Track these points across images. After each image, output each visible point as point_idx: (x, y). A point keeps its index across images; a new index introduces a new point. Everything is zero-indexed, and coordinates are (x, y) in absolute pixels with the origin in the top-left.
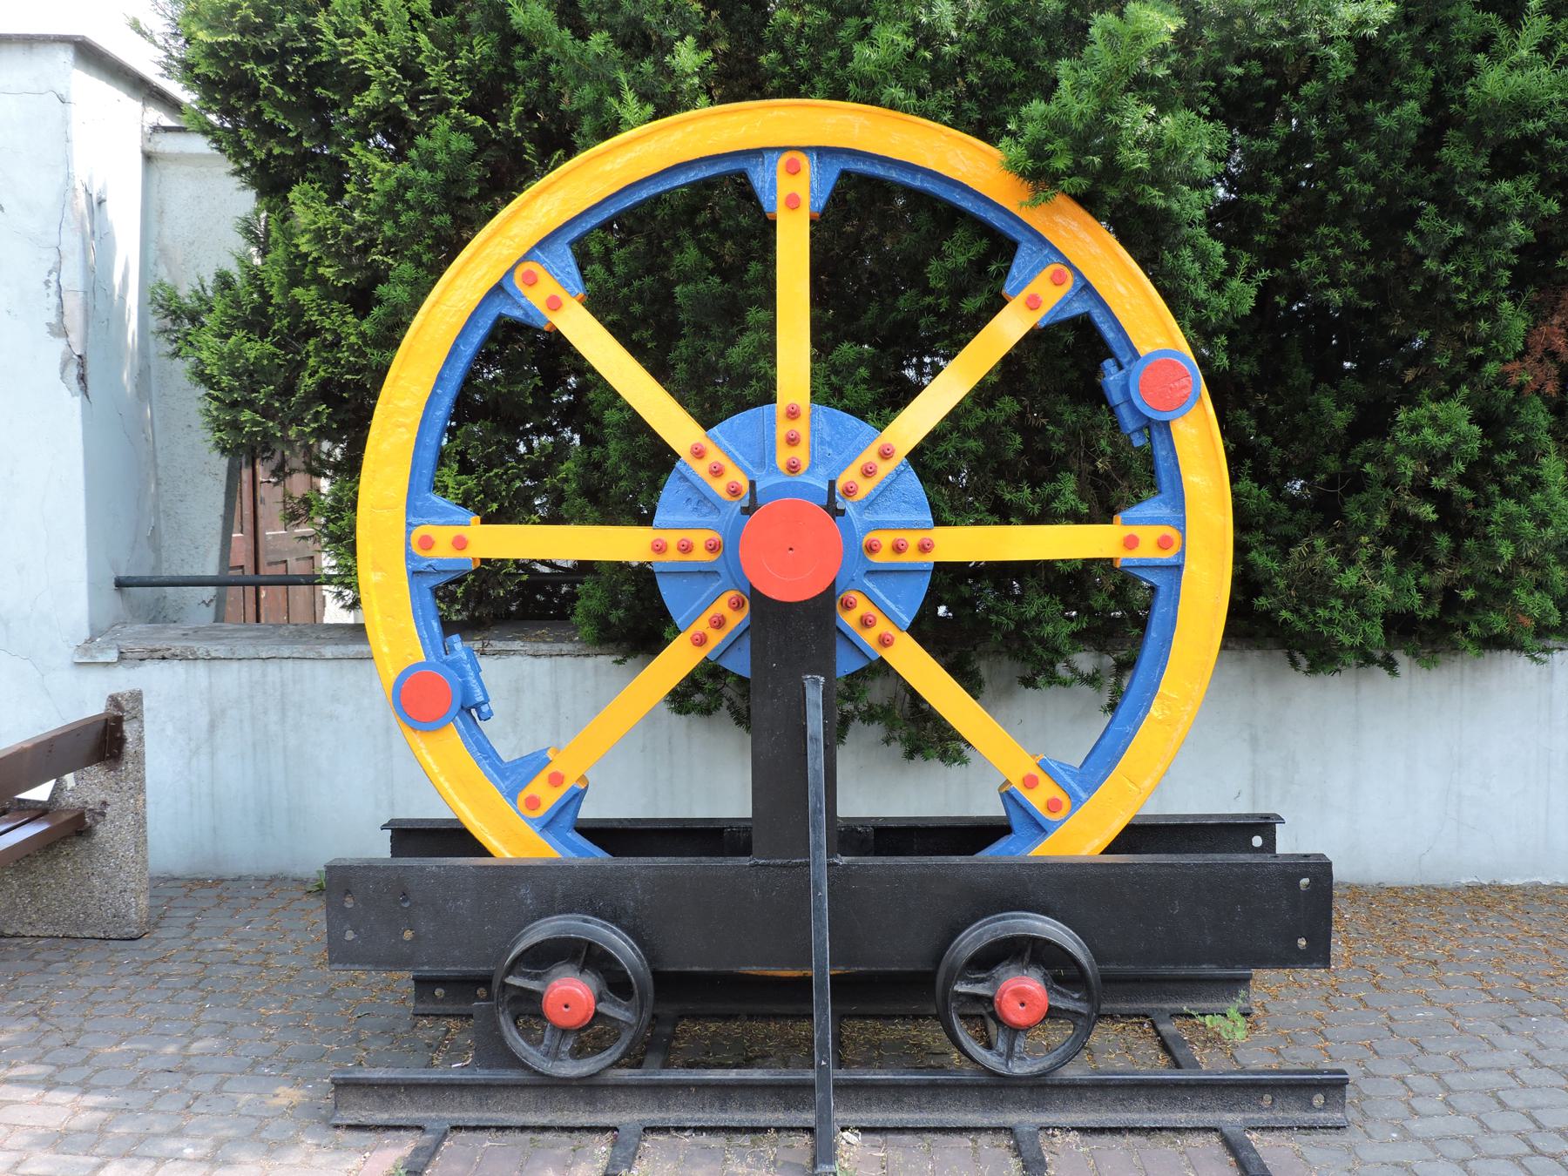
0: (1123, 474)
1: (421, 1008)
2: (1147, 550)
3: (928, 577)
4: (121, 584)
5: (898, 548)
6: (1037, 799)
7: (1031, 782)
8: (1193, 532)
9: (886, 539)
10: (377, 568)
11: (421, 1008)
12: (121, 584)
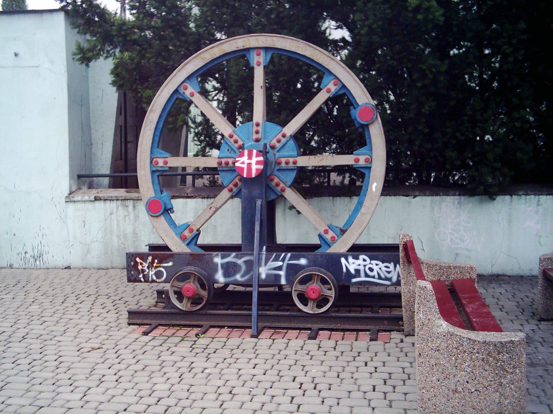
0: (355, 140)
1: (159, 300)
2: (362, 162)
3: (295, 172)
4: (79, 177)
5: (287, 163)
6: (328, 237)
7: (326, 232)
8: (376, 156)
9: (283, 160)
10: (148, 188)
11: (159, 300)
12: (79, 177)
